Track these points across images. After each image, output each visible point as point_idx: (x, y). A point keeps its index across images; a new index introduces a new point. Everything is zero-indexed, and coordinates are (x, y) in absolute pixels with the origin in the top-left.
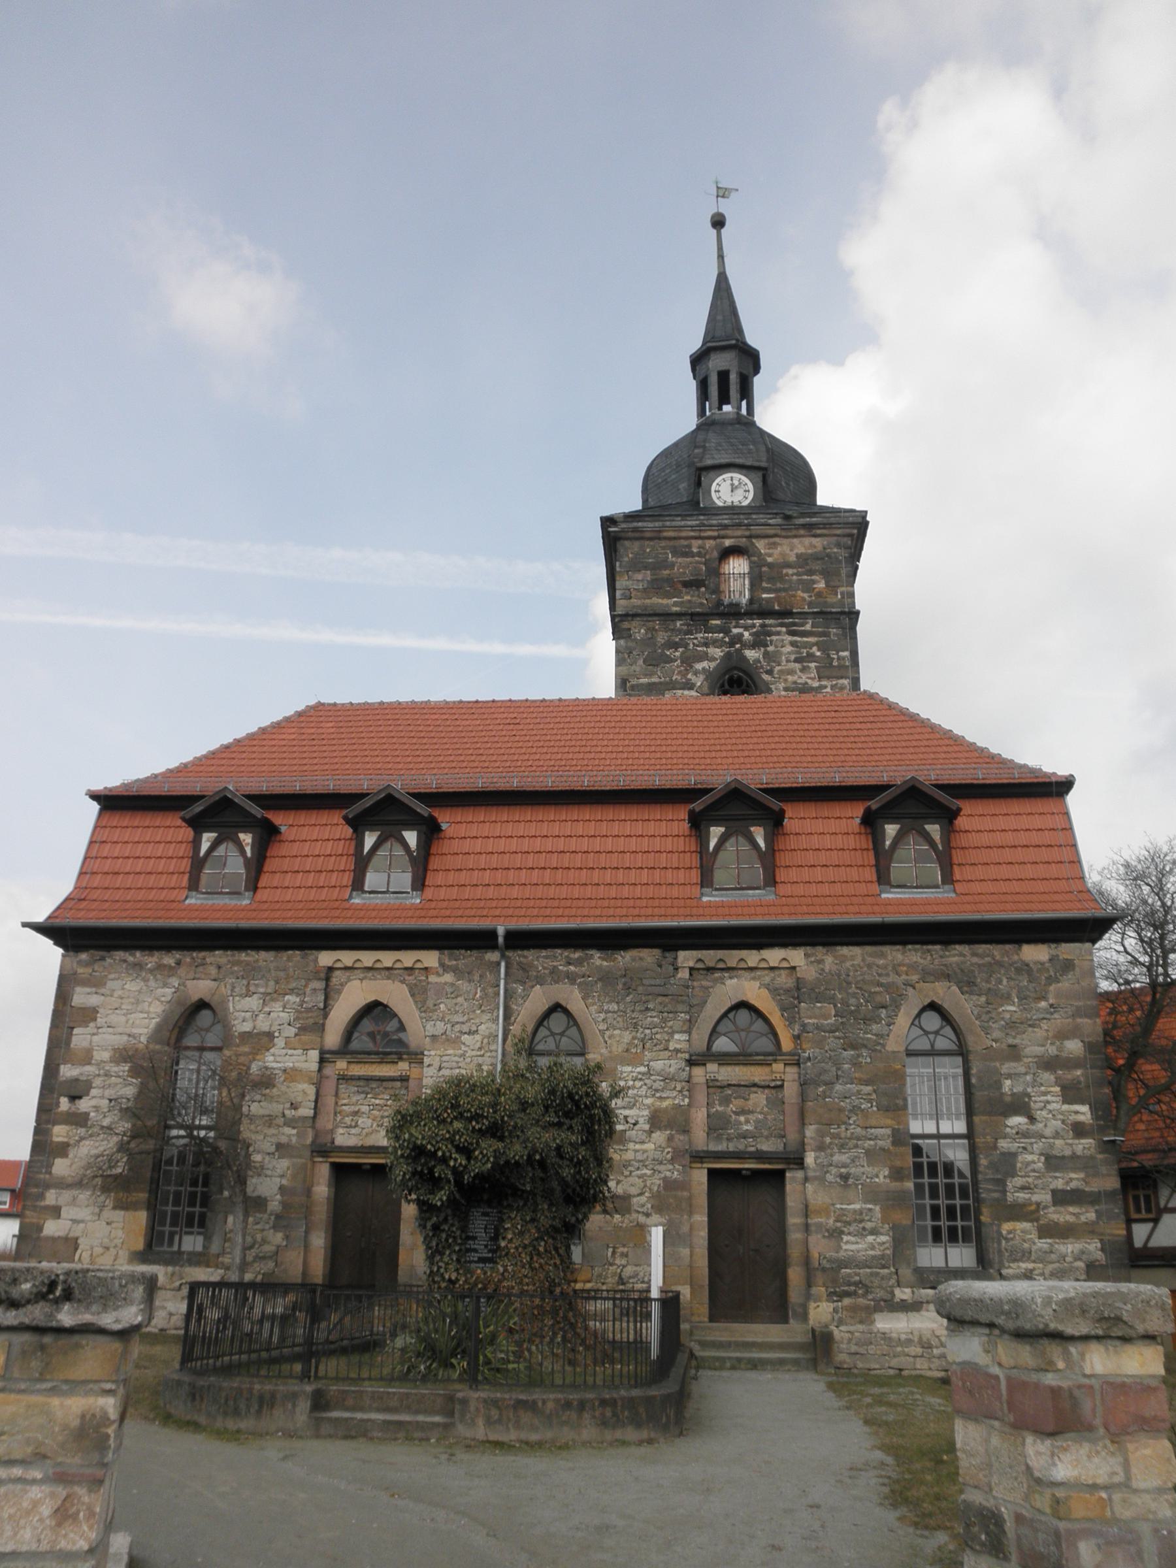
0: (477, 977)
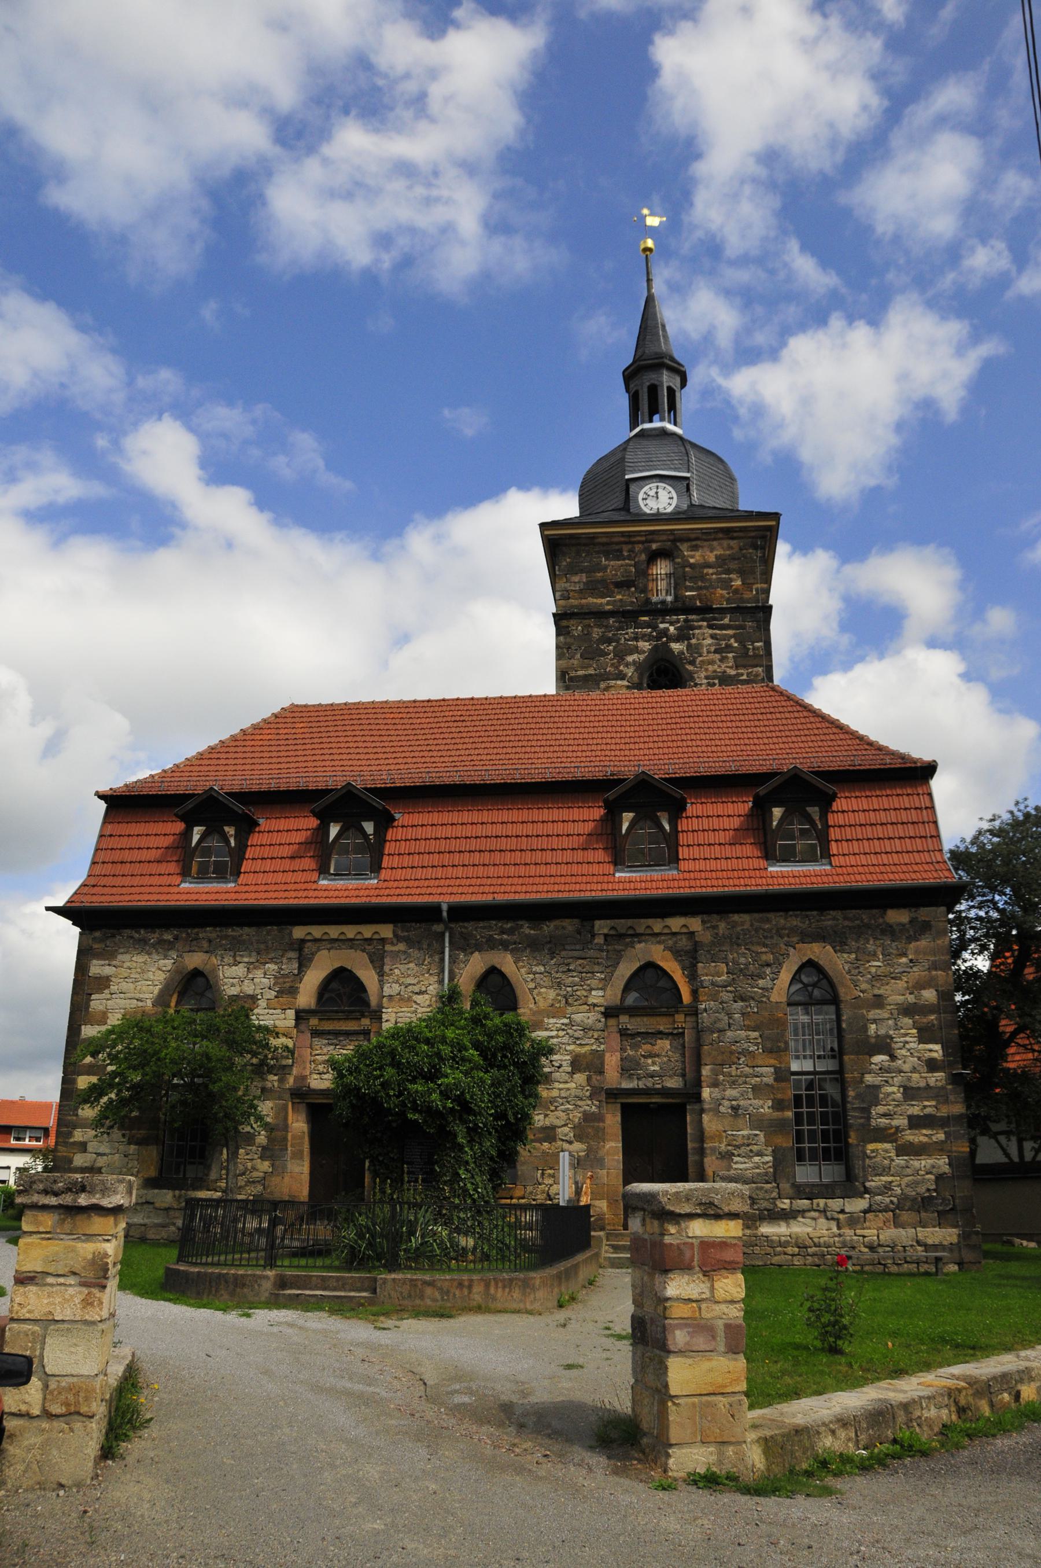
0: (425, 946)
